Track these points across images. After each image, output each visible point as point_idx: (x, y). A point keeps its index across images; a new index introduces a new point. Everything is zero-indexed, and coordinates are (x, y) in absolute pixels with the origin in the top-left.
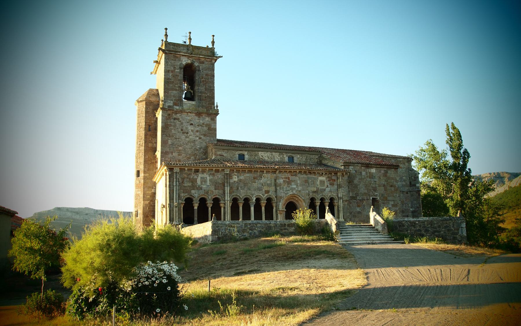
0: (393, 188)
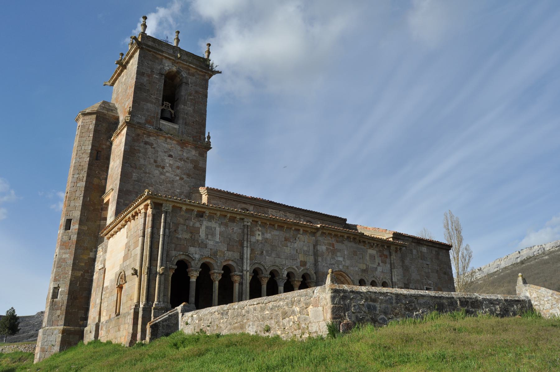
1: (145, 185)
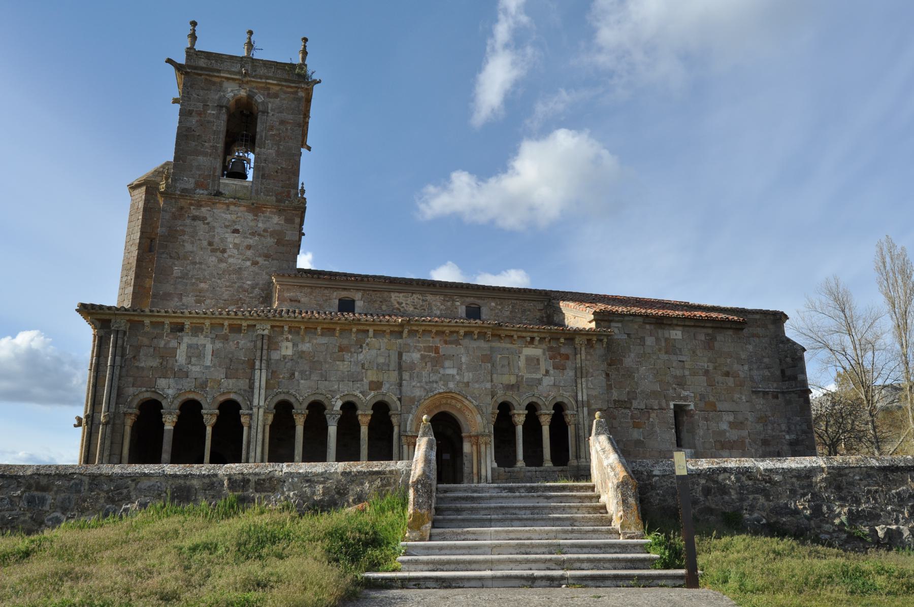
1: (194, 281)
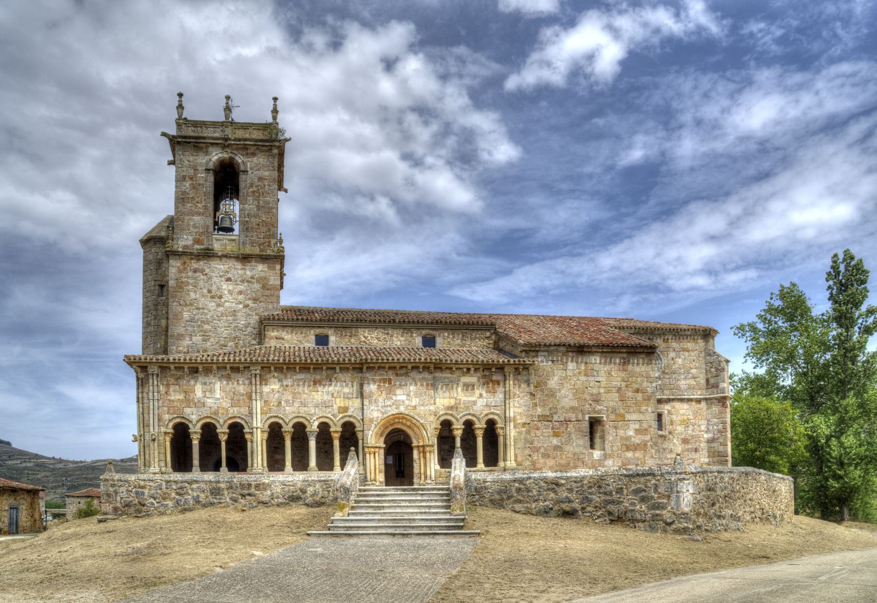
0: (640, 395)
1: (199, 323)
